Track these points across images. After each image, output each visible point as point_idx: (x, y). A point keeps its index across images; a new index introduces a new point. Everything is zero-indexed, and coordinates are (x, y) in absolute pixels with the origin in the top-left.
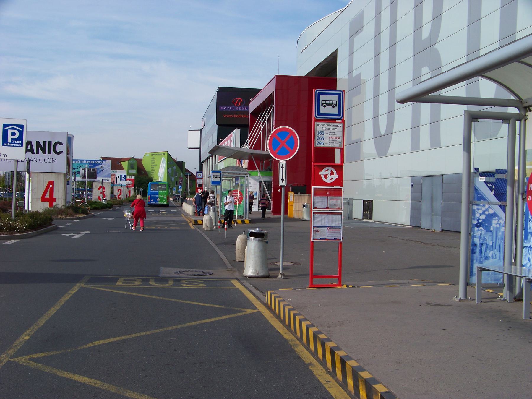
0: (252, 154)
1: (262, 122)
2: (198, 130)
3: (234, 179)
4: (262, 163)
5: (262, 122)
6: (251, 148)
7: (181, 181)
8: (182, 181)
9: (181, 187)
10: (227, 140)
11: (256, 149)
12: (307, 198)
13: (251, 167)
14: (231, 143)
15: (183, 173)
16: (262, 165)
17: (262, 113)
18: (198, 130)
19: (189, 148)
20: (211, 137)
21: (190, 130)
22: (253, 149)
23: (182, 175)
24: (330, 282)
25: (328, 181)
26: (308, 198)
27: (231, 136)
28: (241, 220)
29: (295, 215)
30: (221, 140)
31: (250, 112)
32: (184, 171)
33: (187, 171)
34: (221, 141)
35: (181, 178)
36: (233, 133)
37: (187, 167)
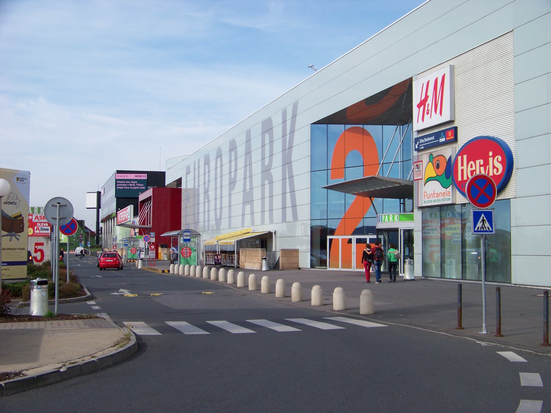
0: (141, 227)
1: (146, 213)
2: (95, 192)
3: (132, 242)
4: (147, 230)
5: (146, 213)
6: (140, 224)
7: (81, 237)
8: (82, 237)
9: (89, 244)
10: (124, 210)
11: (143, 225)
12: (261, 252)
13: (140, 234)
14: (127, 214)
15: (83, 230)
16: (147, 232)
17: (146, 202)
18: (95, 192)
19: (87, 208)
20: (111, 205)
21: (88, 193)
22: (142, 224)
23: (82, 232)
24: (154, 265)
25: (152, 248)
26: (261, 251)
27: (127, 208)
28: (151, 196)
29: (162, 259)
30: (119, 209)
31: (139, 201)
32: (84, 227)
33: (86, 228)
34: (119, 210)
35: (81, 234)
36: (129, 207)
37: (86, 224)
